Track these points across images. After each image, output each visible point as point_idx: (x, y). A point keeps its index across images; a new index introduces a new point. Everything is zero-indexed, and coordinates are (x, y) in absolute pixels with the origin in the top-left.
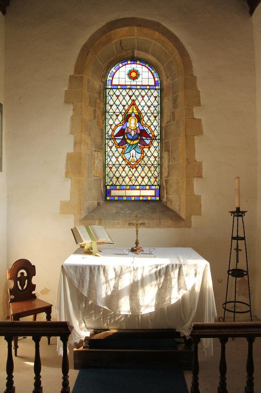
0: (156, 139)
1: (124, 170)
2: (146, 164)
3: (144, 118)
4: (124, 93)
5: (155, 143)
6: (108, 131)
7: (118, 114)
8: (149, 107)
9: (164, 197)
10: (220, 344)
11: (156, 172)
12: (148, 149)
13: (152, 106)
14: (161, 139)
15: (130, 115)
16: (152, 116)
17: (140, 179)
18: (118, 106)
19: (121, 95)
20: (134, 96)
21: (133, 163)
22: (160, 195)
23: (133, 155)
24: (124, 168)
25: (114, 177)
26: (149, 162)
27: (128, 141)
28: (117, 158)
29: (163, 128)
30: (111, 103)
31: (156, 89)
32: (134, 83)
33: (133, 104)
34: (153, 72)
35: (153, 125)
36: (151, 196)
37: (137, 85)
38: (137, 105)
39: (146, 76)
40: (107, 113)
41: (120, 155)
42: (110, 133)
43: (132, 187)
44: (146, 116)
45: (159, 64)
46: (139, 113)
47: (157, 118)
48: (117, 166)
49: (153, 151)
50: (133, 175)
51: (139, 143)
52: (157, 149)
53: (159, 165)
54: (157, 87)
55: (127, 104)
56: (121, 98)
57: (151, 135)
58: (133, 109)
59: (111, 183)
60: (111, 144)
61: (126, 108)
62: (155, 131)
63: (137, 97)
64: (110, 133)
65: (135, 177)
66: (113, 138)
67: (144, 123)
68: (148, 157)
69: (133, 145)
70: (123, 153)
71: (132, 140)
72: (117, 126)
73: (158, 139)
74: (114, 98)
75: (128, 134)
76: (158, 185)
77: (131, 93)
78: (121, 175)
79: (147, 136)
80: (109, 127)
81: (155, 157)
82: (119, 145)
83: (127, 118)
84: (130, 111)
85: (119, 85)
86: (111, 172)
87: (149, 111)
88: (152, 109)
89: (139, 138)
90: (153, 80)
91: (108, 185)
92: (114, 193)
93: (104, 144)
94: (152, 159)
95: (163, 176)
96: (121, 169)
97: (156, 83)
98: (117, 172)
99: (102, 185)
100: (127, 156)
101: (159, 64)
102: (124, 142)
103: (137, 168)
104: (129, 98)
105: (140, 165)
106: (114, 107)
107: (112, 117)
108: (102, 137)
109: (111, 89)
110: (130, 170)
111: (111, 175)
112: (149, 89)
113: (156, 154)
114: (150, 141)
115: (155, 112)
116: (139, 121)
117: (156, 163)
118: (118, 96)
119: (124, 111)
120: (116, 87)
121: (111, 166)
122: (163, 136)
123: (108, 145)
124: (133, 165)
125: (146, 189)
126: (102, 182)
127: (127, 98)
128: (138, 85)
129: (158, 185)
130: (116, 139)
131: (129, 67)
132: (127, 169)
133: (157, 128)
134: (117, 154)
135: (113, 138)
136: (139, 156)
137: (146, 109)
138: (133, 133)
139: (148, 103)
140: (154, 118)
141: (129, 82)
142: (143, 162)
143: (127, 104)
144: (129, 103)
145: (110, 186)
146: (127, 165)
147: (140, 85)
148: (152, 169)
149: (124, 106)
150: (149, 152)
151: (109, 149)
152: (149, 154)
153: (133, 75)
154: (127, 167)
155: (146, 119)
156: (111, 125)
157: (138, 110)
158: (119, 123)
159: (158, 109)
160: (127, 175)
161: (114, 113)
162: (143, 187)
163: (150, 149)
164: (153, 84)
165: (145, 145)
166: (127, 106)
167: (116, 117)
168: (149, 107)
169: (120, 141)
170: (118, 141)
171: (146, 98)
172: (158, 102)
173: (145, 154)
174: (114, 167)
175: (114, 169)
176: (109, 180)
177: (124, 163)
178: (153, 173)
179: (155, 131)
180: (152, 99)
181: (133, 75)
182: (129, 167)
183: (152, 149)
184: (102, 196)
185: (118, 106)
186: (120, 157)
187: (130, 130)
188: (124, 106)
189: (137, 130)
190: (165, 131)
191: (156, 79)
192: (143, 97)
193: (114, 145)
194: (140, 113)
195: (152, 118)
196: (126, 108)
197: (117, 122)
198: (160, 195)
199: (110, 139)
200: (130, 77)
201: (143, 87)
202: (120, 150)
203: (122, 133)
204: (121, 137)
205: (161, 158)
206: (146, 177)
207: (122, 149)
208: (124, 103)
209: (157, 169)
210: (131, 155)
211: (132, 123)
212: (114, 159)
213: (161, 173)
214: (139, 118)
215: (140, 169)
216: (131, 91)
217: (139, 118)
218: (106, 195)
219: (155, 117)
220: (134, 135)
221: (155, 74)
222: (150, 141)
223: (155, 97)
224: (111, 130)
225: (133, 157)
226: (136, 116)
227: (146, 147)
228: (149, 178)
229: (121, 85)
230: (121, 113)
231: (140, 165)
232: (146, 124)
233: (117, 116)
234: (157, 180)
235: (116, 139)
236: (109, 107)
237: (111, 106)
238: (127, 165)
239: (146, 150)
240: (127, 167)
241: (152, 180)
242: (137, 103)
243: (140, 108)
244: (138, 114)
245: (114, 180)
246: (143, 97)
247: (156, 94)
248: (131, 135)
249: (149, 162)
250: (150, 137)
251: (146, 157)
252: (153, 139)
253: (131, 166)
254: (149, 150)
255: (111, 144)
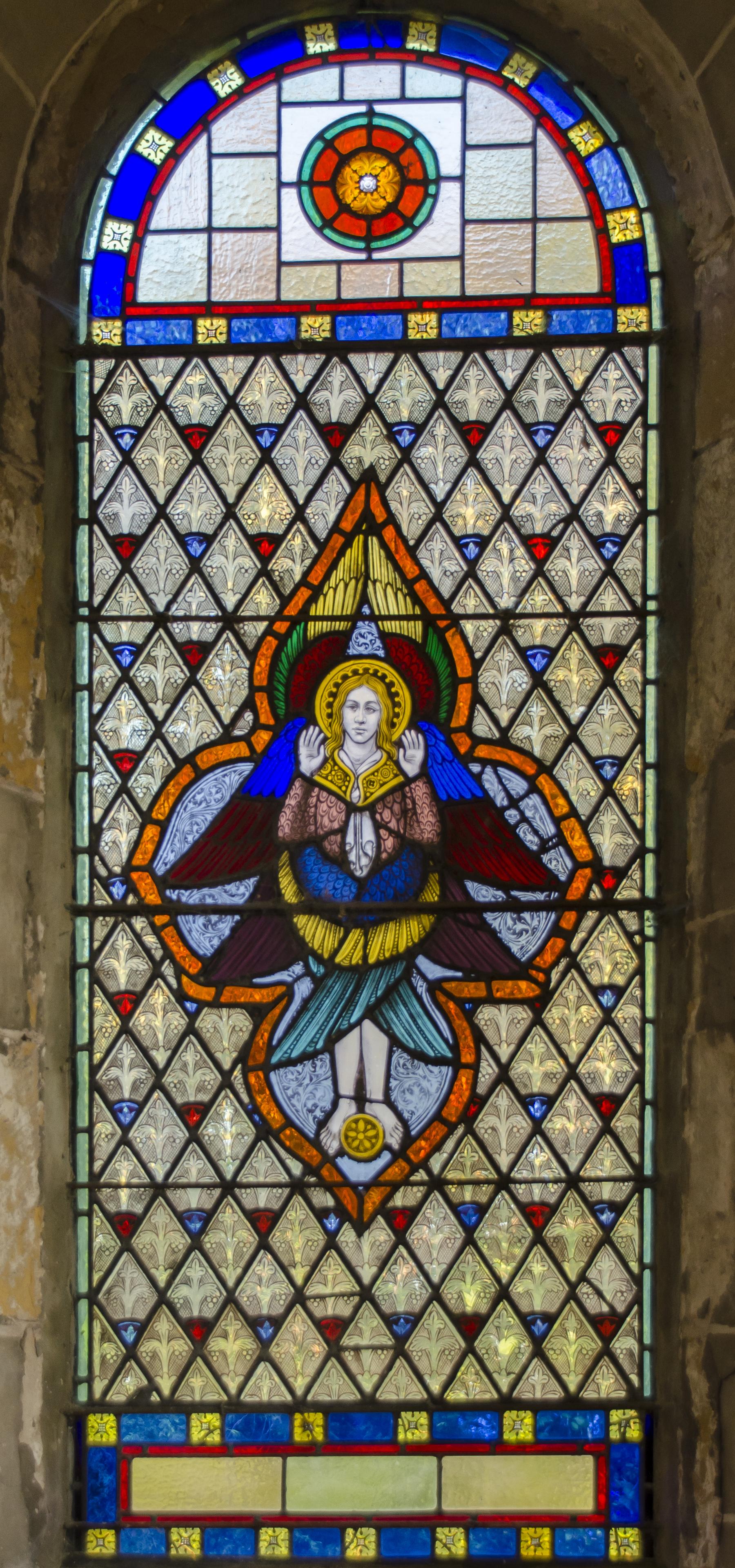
0: (609, 906)
1: (264, 1245)
2: (504, 1182)
3: (486, 677)
4: (265, 393)
5: (607, 953)
6: (96, 830)
7: (196, 631)
8: (540, 547)
9: (692, 1532)
10: (291, 406)
11: (606, 1262)
12: (523, 1014)
13: (575, 541)
14: (668, 909)
15: (333, 648)
16: (574, 652)
17: (434, 1341)
18: (196, 546)
19: (232, 430)
20: (371, 430)
21: (358, 1172)
22: (648, 1500)
23: (365, 1078)
24: (263, 1222)
25: (164, 1324)
26: (539, 1156)
27: (315, 931)
28: (194, 1115)
29: (686, 777)
30: (127, 512)
31: (613, 342)
32: (371, 282)
33: (368, 517)
34: (584, 138)
35: (584, 748)
36: (556, 1521)
37: (403, 306)
38: (411, 531)
39: (503, 183)
40: (83, 629)
41: (226, 1083)
42: (118, 840)
43: (256, 1432)
44: (505, 655)
45: (653, 41)
46: (428, 620)
47: (627, 673)
48: (193, 1199)
49: (585, 1030)
50: (366, 1294)
51: (426, 946)
52: (626, 1013)
53: (639, 1181)
54: (630, 318)
55: (300, 515)
56: (231, 454)
57: (557, 863)
58: (364, 577)
59: (130, 1383)
60: (123, 967)
61: (290, 564)
62: (610, 818)
63: (405, 437)
64: (118, 840)
65: (390, 1321)
66: (147, 899)
67: (482, 727)
68: (525, 1101)
69: (360, 972)
70: (256, 1060)
71: (365, 909)
72: (190, 767)
73: (637, 906)
74: (162, 455)
75: (311, 859)
76: (633, 1399)
77: (337, 400)
78: (231, 1300)
79: (520, 869)
80: (105, 778)
81: (606, 1105)
82: (222, 973)
83: (298, 672)
84: (336, 600)
85: (210, 309)
86: (127, 1268)
87: (540, 599)
88: (574, 565)
89: (432, 895)
90: (586, 229)
91: (101, 1406)
92: (158, 1485)
93: (57, 958)
94: (571, 1121)
95: (691, 1305)
96: (231, 1234)
97: (623, 271)
98: (195, 1269)
99: (33, 1402)
100: (299, 1092)
101: (653, 41)
102: (261, 943)
103: (401, 1222)
104: (322, 455)
105: (437, 1184)
106: (160, 560)
107: (142, 673)
108: (30, 885)
109: (126, 353)
110: (331, 1243)
111: (131, 1297)
112: (542, 344)
113: (607, 1069)
114: (542, 921)
115: (609, 599)
116: (430, 717)
117: (607, 1162)
118: (196, 437)
119: (263, 600)
120: (174, 333)
121: (124, 1201)
122: (694, 867)
123: (95, 980)
124: (360, 1190)
125: (498, 1447)
126: (34, 1370)
127: (302, 451)
128: (421, 304)
129: (633, 1399)
130: (175, 910)
131: (310, 105)
132: (297, 1234)
133: (628, 784)
134: (192, 1079)
135: (153, 898)
136: (425, 1091)
137: (505, 566)
138: (363, 844)
139: (541, 506)
140: (594, 675)
141: (311, 259)
142: (470, 1153)
143: (300, 515)
144: (325, 512)
145: (118, 1410)
146: (297, 1187)
147: (441, 305)
148: (572, 1226)
149: (265, 545)
150: (537, 1045)
151: (108, 1022)
152: (537, 1070)
153: (369, 185)
154: (297, 1211)
155: (503, 679)
156: (126, 762)
157: (414, 583)
158: (214, 731)
159: (642, 564)
160: (299, 1298)
161: (161, 620)
162: (459, 1431)
163: (553, 1015)
164: (588, 281)
165: (492, 966)
166: (297, 542)
167: (179, 675)
168: (540, 547)
169: (226, 926)
170: (206, 936)
171: (506, 451)
172: (637, 488)
173: (488, 1070)
174: (161, 1216)
175: (161, 1237)
176: (111, 1351)
177: (264, 1166)
178: (572, 1270)
179: (610, 818)
180: (576, 456)
181: (369, 185)
182: (321, 1214)
183: (571, 1012)
184: (35, 1526)
185: (196, 546)
186: (227, 1109)
187: (329, 814)
188: (265, 545)
189: (408, 814)
190: (711, 810)
191: (624, 228)
192: (474, 434)
193: (156, 973)
194: (441, 619)
195: (574, 675)
196: (290, 564)
197: (190, 729)
198: (648, 1500)
199: (121, 912)
200: (333, 216)
201: (475, 323)
202: (227, 1028)
203: (239, 841)
204: (239, 892)
205: (670, 1106)
206: (505, 1315)
207: (241, 1020)
208: (267, 508)
209: (627, 1227)
210: (347, 1087)
211: (360, 731)
212: (159, 1132)
213: (666, 1271)
214: (430, 673)
215: (435, 1232)
216: (338, 374)
217: (430, 673)
218: (78, 1511)
219: (608, 657)
220: (377, 865)
221: (603, 169)
222: (542, 921)
223: (611, 434)
224: (124, 815)
225: (361, 1098)
226: (397, 649)
227: (503, 988)
228: (537, 1327)
229: (231, 311)
230: (230, 621)
231: (437, 1184)
232: (504, 740)
233: (194, 655)
234: (624, 1344)
235: (175, 910)
236: (107, 563)
237: (127, 547)
238: (297, 1187)
239: (501, 1022)
240: (297, 1211)
241: (572, 1345)
242: (408, 506)
243: (440, 562)
244: (414, 630)
245: (166, 1347)
246: (474, 434)
247: (613, 394)
248: (341, 861)
249: (539, 1156)
250: (544, 879)
251: (503, 1099)
252: (583, 906)
253: (346, 1195)
254: (538, 1021)
255: (123, 967)
